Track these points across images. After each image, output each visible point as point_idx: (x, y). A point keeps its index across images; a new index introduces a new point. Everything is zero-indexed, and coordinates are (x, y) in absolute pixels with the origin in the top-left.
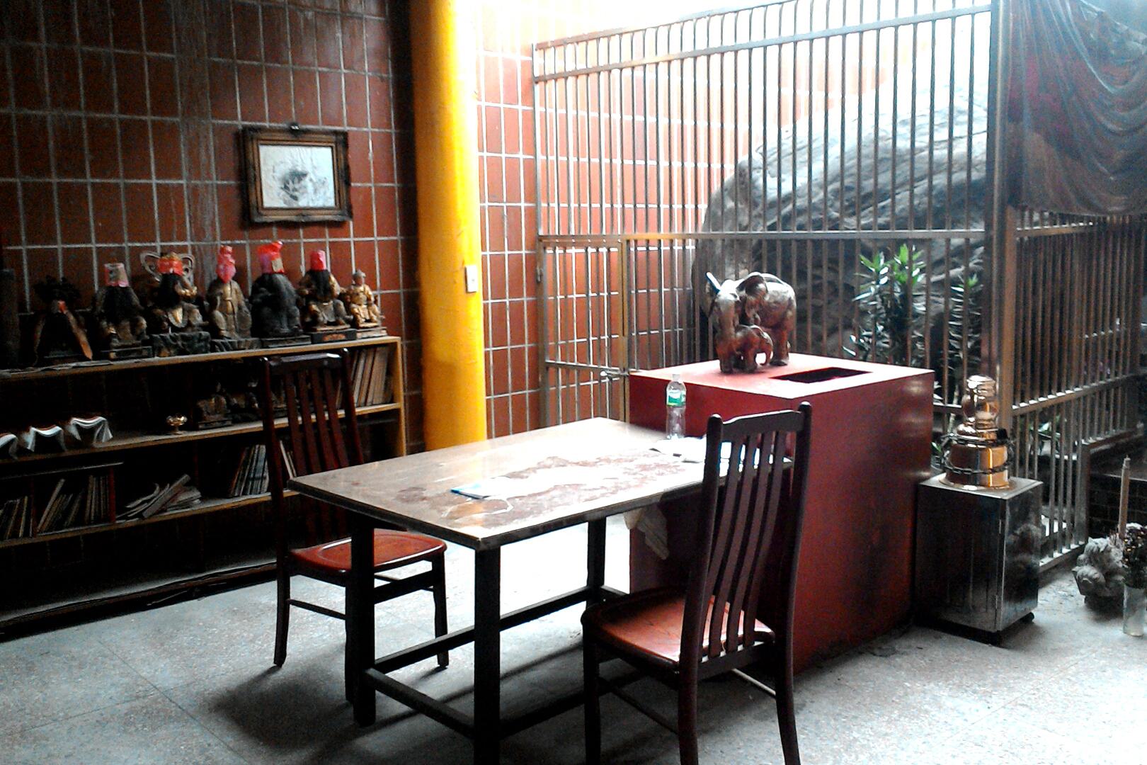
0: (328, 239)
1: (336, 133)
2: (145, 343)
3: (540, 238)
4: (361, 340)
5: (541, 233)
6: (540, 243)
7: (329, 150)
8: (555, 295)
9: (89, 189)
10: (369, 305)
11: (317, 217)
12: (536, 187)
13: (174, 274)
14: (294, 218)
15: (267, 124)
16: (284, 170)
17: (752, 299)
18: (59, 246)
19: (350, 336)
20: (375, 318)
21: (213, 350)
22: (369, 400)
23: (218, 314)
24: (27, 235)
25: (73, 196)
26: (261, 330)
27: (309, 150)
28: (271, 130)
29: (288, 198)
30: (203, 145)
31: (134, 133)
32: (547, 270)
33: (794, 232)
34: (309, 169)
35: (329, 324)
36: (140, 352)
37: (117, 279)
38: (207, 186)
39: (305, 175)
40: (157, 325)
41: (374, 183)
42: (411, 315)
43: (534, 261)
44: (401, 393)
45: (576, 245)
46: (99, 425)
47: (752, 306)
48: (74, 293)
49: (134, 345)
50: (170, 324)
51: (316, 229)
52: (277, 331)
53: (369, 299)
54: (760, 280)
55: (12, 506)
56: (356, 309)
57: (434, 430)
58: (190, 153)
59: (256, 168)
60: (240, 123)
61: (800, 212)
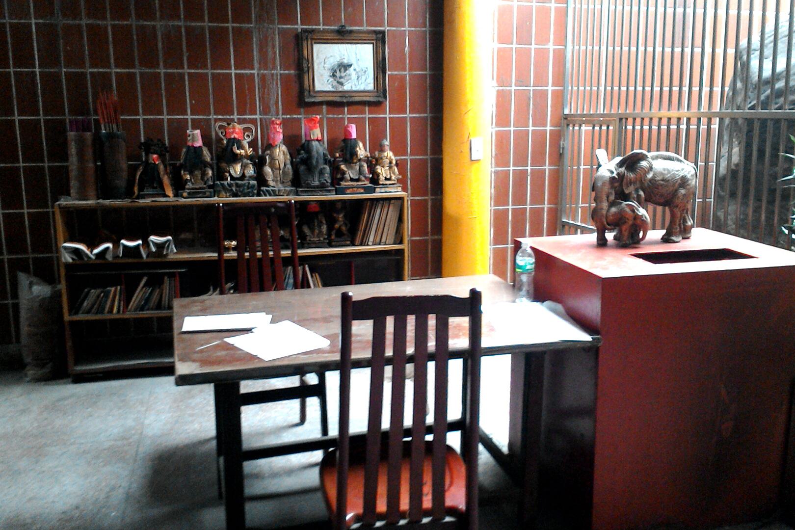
0: (367, 116)
1: (375, 32)
2: (210, 187)
3: (566, 117)
4: (379, 193)
5: (567, 112)
6: (567, 120)
7: (371, 46)
8: (579, 165)
9: (186, 77)
10: (390, 167)
11: (357, 99)
12: (564, 74)
13: (234, 138)
14: (338, 99)
15: (321, 27)
16: (333, 61)
17: (631, 175)
18: (165, 117)
19: (368, 190)
20: (393, 178)
21: (259, 195)
22: (383, 240)
23: (268, 169)
24: (143, 109)
25: (175, 81)
26: (297, 182)
27: (354, 46)
28: (324, 31)
29: (335, 83)
30: (270, 44)
31: (219, 37)
32: (566, 143)
33: (773, 110)
34: (353, 61)
35: (352, 180)
36: (205, 193)
37: (193, 140)
38: (272, 75)
39: (350, 66)
40: (220, 175)
41: (407, 73)
42: (431, 177)
43: (557, 136)
44: (406, 239)
45: (587, 123)
46: (166, 242)
47: (631, 183)
48: (170, 152)
49: (200, 188)
50: (230, 175)
51: (360, 107)
52: (308, 184)
53: (391, 163)
54: (643, 157)
55: (109, 291)
56: (379, 169)
57: (446, 268)
58: (261, 50)
59: (310, 60)
60: (299, 27)
61: (779, 94)
